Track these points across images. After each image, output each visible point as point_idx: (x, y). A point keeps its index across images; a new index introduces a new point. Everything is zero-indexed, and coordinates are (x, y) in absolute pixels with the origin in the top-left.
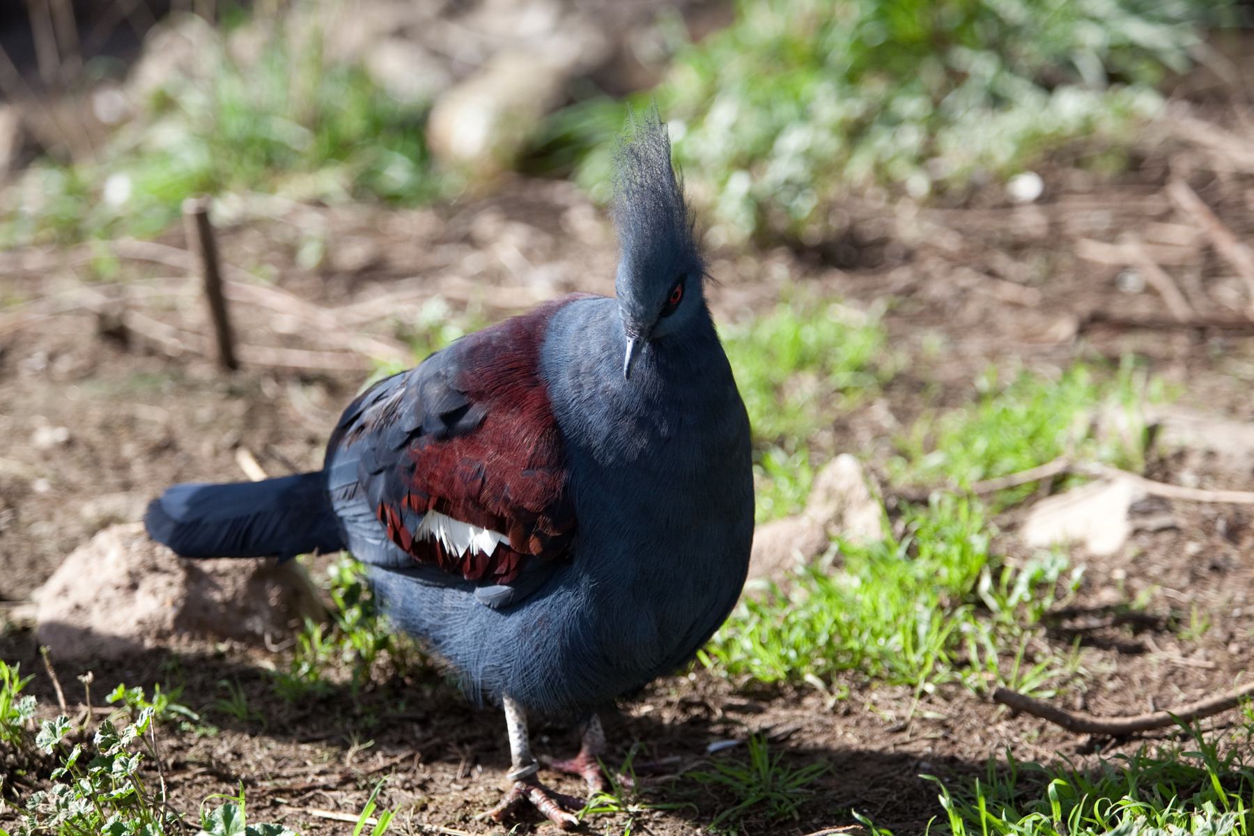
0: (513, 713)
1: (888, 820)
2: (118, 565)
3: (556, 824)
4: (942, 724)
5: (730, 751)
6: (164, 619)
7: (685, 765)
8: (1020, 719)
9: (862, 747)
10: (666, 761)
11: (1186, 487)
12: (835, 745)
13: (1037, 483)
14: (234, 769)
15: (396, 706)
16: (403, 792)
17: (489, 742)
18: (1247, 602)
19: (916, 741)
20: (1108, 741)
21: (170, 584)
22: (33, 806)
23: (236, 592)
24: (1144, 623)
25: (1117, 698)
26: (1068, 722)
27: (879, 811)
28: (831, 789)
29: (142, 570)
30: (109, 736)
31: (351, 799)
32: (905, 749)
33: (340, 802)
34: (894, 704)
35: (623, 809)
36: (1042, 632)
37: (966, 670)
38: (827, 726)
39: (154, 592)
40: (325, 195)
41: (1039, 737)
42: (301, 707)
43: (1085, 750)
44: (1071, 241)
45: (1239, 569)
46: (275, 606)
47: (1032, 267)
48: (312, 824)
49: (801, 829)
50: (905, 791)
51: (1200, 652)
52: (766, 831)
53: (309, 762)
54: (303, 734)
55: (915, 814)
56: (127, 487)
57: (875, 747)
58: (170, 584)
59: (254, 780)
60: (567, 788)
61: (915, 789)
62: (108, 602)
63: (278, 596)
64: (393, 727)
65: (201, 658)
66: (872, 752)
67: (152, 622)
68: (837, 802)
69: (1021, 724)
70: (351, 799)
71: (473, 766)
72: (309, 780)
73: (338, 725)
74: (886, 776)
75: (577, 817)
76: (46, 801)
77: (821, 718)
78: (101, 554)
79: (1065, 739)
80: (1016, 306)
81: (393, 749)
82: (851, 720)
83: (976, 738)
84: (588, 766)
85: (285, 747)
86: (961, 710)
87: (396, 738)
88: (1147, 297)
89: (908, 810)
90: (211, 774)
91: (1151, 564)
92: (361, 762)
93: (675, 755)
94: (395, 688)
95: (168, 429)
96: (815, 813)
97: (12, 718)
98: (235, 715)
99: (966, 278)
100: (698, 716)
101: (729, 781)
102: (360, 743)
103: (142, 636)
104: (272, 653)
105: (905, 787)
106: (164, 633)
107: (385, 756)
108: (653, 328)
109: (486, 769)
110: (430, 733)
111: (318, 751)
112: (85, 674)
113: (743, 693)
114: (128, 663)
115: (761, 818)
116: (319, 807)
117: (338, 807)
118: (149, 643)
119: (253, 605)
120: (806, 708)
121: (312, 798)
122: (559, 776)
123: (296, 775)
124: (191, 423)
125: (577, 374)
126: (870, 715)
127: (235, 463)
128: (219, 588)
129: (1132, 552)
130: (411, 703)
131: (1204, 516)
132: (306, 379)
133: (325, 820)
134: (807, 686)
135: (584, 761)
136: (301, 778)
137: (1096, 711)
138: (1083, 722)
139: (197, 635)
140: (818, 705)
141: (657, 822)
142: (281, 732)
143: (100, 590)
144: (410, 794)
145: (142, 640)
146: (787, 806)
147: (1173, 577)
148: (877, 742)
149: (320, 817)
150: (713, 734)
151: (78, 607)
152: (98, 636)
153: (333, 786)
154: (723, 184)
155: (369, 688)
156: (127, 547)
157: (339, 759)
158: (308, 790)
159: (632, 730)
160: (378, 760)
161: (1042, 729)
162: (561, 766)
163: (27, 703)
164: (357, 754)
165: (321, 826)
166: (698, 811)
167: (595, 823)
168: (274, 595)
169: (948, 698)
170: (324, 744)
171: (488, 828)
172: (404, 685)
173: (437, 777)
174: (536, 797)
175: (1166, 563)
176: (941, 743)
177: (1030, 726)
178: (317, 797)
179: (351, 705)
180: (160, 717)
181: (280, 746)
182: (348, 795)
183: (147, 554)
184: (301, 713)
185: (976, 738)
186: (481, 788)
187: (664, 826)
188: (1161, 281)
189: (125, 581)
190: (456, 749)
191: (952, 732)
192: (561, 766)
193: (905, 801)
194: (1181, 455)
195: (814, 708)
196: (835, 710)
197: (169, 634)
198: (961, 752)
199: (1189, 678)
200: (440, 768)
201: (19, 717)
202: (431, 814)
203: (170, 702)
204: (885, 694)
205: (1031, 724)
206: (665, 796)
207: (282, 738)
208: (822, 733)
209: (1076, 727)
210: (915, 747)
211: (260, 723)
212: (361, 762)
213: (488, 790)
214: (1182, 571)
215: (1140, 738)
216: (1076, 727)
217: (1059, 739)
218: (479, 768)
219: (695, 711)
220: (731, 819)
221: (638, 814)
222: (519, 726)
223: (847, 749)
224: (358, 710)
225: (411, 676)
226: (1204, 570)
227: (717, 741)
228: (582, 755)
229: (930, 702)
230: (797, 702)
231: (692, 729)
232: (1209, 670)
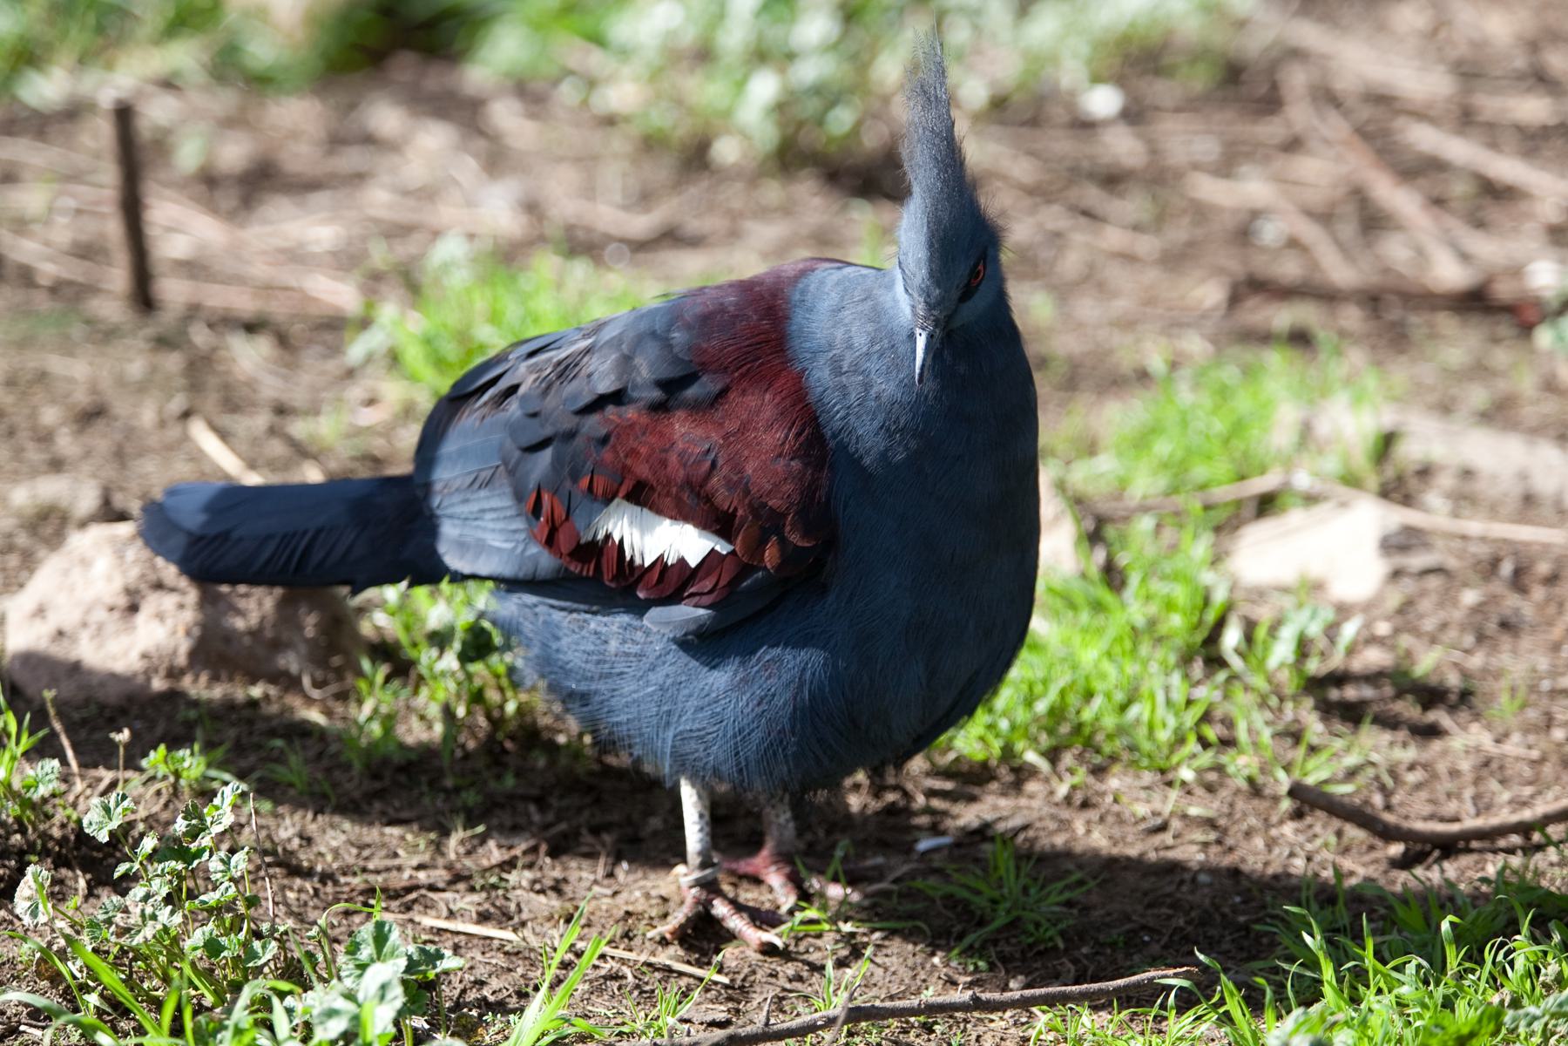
0: (695, 798)
1: (1177, 951)
2: (109, 579)
3: (748, 945)
4: (1211, 823)
5: (946, 852)
6: (175, 653)
8: (1308, 820)
9: (1115, 851)
10: (870, 862)
11: (1434, 512)
12: (1078, 848)
13: (1239, 503)
14: (305, 859)
15: (499, 777)
16: (532, 895)
18: (1554, 673)
19: (1182, 844)
21: (181, 606)
22: (105, 917)
23: (263, 619)
24: (1431, 695)
25: (1424, 795)
26: (1380, 828)
27: (1165, 939)
28: (1094, 907)
29: (143, 586)
30: (194, 822)
31: (468, 903)
32: (1171, 855)
34: (1143, 794)
37: (1232, 752)
39: (160, 617)
40: (176, 74)
41: (1339, 844)
42: (376, 776)
43: (1405, 863)
44: (1179, 175)
45: (1534, 628)
47: (1133, 206)
48: (424, 937)
50: (1193, 914)
51: (1516, 737)
53: (401, 852)
55: (1210, 944)
56: (57, 465)
57: (1133, 852)
58: (181, 606)
60: (748, 895)
61: (1206, 911)
62: (100, 628)
63: (315, 625)
64: (502, 806)
65: (229, 706)
66: (1128, 859)
67: (160, 657)
68: (1108, 925)
69: (1310, 826)
70: (468, 903)
72: (406, 874)
73: (426, 801)
76: (126, 911)
77: (1054, 810)
78: (85, 563)
79: (1372, 848)
81: (507, 837)
82: (1093, 815)
83: (1259, 842)
84: (773, 868)
85: (365, 830)
86: (1231, 805)
90: (278, 864)
92: (469, 853)
93: (875, 855)
94: (492, 750)
95: (94, 390)
96: (1083, 941)
97: (28, 788)
98: (291, 785)
99: (1054, 217)
100: (893, 803)
102: (465, 830)
103: (148, 673)
104: (315, 700)
105: (1192, 908)
107: (500, 847)
108: (949, 318)
109: (634, 867)
110: (550, 817)
111: (409, 837)
112: (120, 731)
113: (946, 774)
114: (135, 710)
115: (1014, 945)
116: (426, 913)
117: (451, 915)
118: (158, 684)
119: (285, 636)
120: (1031, 797)
121: (415, 901)
122: (734, 880)
123: (388, 869)
124: (121, 382)
125: (837, 371)
126: (1116, 808)
129: (1394, 599)
130: (518, 775)
131: (1474, 555)
132: (252, 327)
133: (440, 931)
135: (768, 861)
136: (395, 873)
137: (1403, 811)
139: (224, 675)
141: (878, 947)
142: (354, 809)
143: (88, 611)
144: (542, 898)
145: (149, 679)
146: (1046, 930)
147: (1452, 634)
148: (1132, 844)
149: (432, 928)
150: (919, 828)
151: (61, 633)
152: (91, 672)
153: (441, 885)
154: (741, 85)
156: (120, 556)
157: (438, 848)
158: (409, 890)
160: (491, 852)
161: (1339, 834)
162: (734, 866)
163: (48, 769)
164: (462, 842)
166: (929, 933)
167: (796, 945)
169: (1210, 788)
170: (415, 827)
171: (660, 948)
172: (505, 751)
173: (573, 876)
174: (720, 909)
176: (1214, 849)
177: (1323, 829)
179: (440, 773)
180: (195, 786)
181: (357, 829)
183: (147, 565)
184: (377, 785)
185: (1259, 842)
186: (638, 894)
187: (889, 951)
188: (1310, 232)
189: (122, 601)
191: (1225, 831)
192: (734, 866)
194: (1425, 472)
195: (1041, 796)
196: (1068, 800)
199: (1509, 772)
200: (573, 864)
201: (37, 787)
203: (209, 765)
205: (1324, 827)
207: (355, 817)
208: (1058, 830)
209: (1388, 834)
211: (325, 796)
212: (469, 853)
213: (647, 896)
214: (1463, 628)
215: (1470, 851)
216: (1388, 834)
218: (625, 865)
221: (852, 935)
223: (1095, 854)
224: (449, 782)
225: (512, 738)
226: (1492, 627)
228: (765, 852)
229: (1189, 793)
230: (1017, 786)
231: (891, 821)
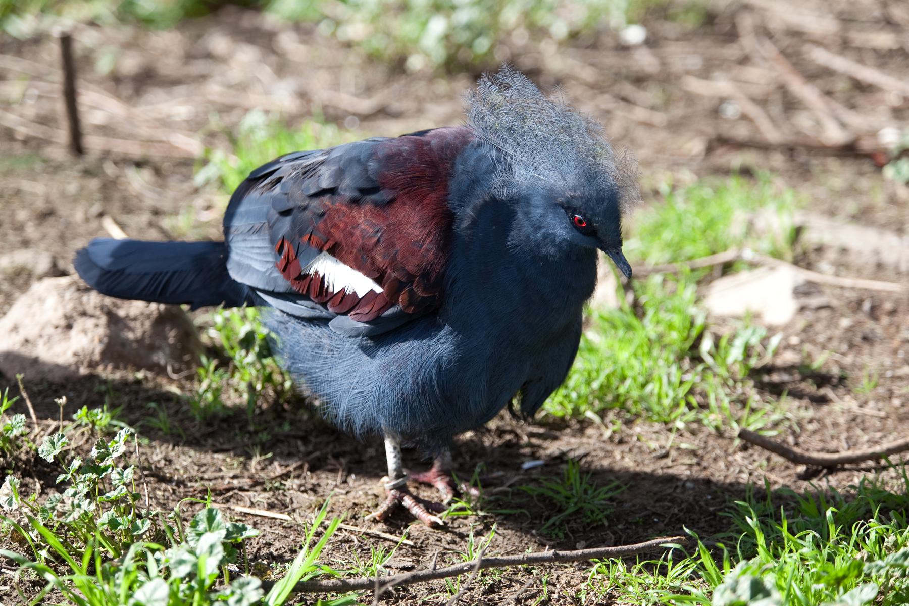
1: (674, 527)
2: (55, 310)
4: (694, 453)
5: (540, 469)
6: (93, 352)
7: (508, 479)
8: (750, 451)
9: (638, 469)
11: (825, 273)
12: (617, 467)
13: (711, 267)
14: (167, 472)
15: (280, 425)
16: (299, 493)
17: (356, 456)
19: (677, 465)
20: (821, 471)
21: (97, 326)
22: (51, 505)
23: (144, 333)
24: (822, 379)
25: (817, 437)
26: (792, 456)
27: (667, 520)
29: (75, 314)
30: (102, 450)
32: (670, 471)
33: (254, 501)
34: (654, 436)
35: (474, 513)
36: (751, 383)
37: (706, 411)
38: (607, 451)
39: (85, 332)
40: (97, 17)
42: (209, 424)
43: (806, 476)
45: (882, 341)
46: (173, 344)
47: (651, 95)
48: (237, 518)
49: (612, 533)
50: (683, 506)
51: (871, 404)
52: (584, 533)
53: (223, 468)
54: (213, 446)
56: (26, 244)
57: (648, 469)
58: (97, 326)
59: (184, 481)
60: (425, 494)
61: (690, 504)
62: (50, 338)
63: (174, 337)
64: (282, 442)
65: (125, 383)
66: (646, 473)
69: (751, 455)
71: (349, 473)
72: (226, 481)
73: (238, 438)
74: (664, 493)
75: (441, 518)
78: (41, 300)
79: (787, 468)
80: (648, 125)
82: (625, 448)
83: (721, 464)
84: (439, 478)
85: (203, 456)
86: (706, 443)
87: (286, 452)
88: (744, 122)
89: (687, 520)
90: (152, 475)
91: (817, 334)
92: (263, 469)
93: (498, 470)
94: (277, 410)
96: (618, 520)
97: (7, 431)
98: (160, 429)
99: (605, 101)
101: (551, 494)
103: (78, 364)
104: (175, 380)
105: (682, 502)
106: (94, 363)
107: (281, 465)
109: (358, 477)
110: (310, 448)
111: (228, 460)
112: (60, 398)
114: (69, 386)
115: (579, 523)
117: (252, 505)
118: (83, 371)
119: (157, 343)
120: (589, 437)
121: (231, 497)
122: (417, 485)
123: (216, 478)
124: (63, 195)
126: (639, 444)
127: (101, 228)
128: (131, 329)
129: (801, 323)
130: (292, 423)
131: (848, 298)
132: (139, 164)
133: (246, 514)
134: (587, 420)
136: (220, 481)
137: (806, 446)
138: (802, 456)
139: (121, 365)
140: (598, 435)
142: (196, 443)
143: (43, 328)
144: (305, 495)
145: (78, 368)
146: (598, 514)
147: (835, 344)
148: (648, 465)
149: (241, 512)
150: (524, 455)
151: (27, 341)
152: (44, 364)
153: (247, 487)
154: (424, 24)
155: (257, 411)
156: (62, 296)
157: (245, 466)
158: (228, 490)
159: (463, 450)
160: (275, 468)
161: (768, 459)
162: (416, 477)
163: (18, 420)
164: (259, 463)
165: (244, 519)
166: (529, 516)
167: (452, 523)
168: (172, 335)
169: (694, 433)
170: (232, 454)
172: (284, 410)
173: (323, 482)
174: (407, 502)
175: (829, 333)
176: (696, 468)
177: (759, 457)
178: (235, 496)
179: (247, 423)
180: (104, 430)
181: (198, 455)
182: (259, 495)
184: (210, 429)
185: (721, 464)
186: (361, 493)
188: (753, 110)
189: (63, 322)
190: (332, 460)
191: (702, 458)
193: (684, 513)
194: (820, 250)
195: (595, 437)
196: (611, 439)
197: (97, 364)
198: (712, 475)
200: (323, 476)
201: (12, 430)
202: (328, 512)
203: (112, 418)
204: (646, 428)
205: (760, 455)
206: (501, 503)
207: (198, 448)
208: (605, 457)
209: (797, 459)
210: (677, 470)
212: (263, 469)
213: (366, 494)
214: (841, 340)
215: (844, 470)
216: (797, 459)
217: (783, 468)
218: (353, 476)
219: (508, 437)
220: (557, 523)
222: (395, 448)
223: (626, 471)
224: (251, 428)
225: (288, 402)
226: (858, 340)
227: (529, 461)
228: (434, 470)
229: (681, 435)
230: (581, 431)
232: (882, 419)
